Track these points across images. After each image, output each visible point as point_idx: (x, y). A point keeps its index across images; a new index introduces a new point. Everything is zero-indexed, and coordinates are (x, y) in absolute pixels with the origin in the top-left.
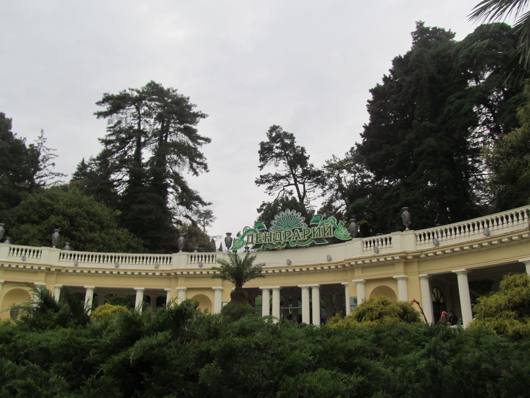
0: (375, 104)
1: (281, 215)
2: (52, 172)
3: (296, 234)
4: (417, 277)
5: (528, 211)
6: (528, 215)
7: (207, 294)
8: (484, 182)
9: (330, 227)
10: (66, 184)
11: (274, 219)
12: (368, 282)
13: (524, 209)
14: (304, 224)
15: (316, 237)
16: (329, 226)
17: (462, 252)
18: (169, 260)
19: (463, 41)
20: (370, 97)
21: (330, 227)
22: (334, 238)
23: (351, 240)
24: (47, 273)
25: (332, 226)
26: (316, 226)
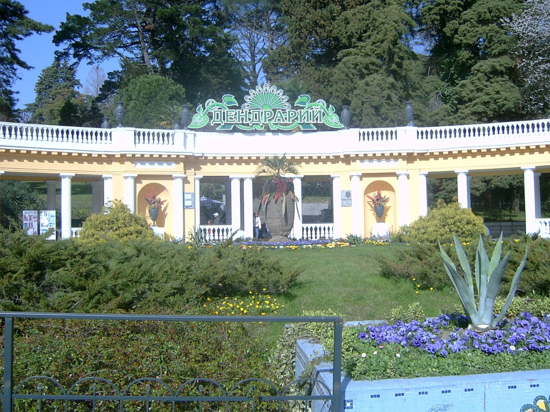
0: (513, 288)
1: (278, 92)
2: (377, 398)
3: (279, 115)
5: (548, 125)
6: (548, 128)
8: (325, 246)
9: (320, 112)
10: (415, 125)
11: (284, 95)
13: (545, 121)
14: (287, 104)
15: (315, 122)
16: (318, 110)
19: (494, 121)
20: (54, 44)
21: (320, 112)
22: (324, 124)
25: (322, 111)
26: (303, 108)
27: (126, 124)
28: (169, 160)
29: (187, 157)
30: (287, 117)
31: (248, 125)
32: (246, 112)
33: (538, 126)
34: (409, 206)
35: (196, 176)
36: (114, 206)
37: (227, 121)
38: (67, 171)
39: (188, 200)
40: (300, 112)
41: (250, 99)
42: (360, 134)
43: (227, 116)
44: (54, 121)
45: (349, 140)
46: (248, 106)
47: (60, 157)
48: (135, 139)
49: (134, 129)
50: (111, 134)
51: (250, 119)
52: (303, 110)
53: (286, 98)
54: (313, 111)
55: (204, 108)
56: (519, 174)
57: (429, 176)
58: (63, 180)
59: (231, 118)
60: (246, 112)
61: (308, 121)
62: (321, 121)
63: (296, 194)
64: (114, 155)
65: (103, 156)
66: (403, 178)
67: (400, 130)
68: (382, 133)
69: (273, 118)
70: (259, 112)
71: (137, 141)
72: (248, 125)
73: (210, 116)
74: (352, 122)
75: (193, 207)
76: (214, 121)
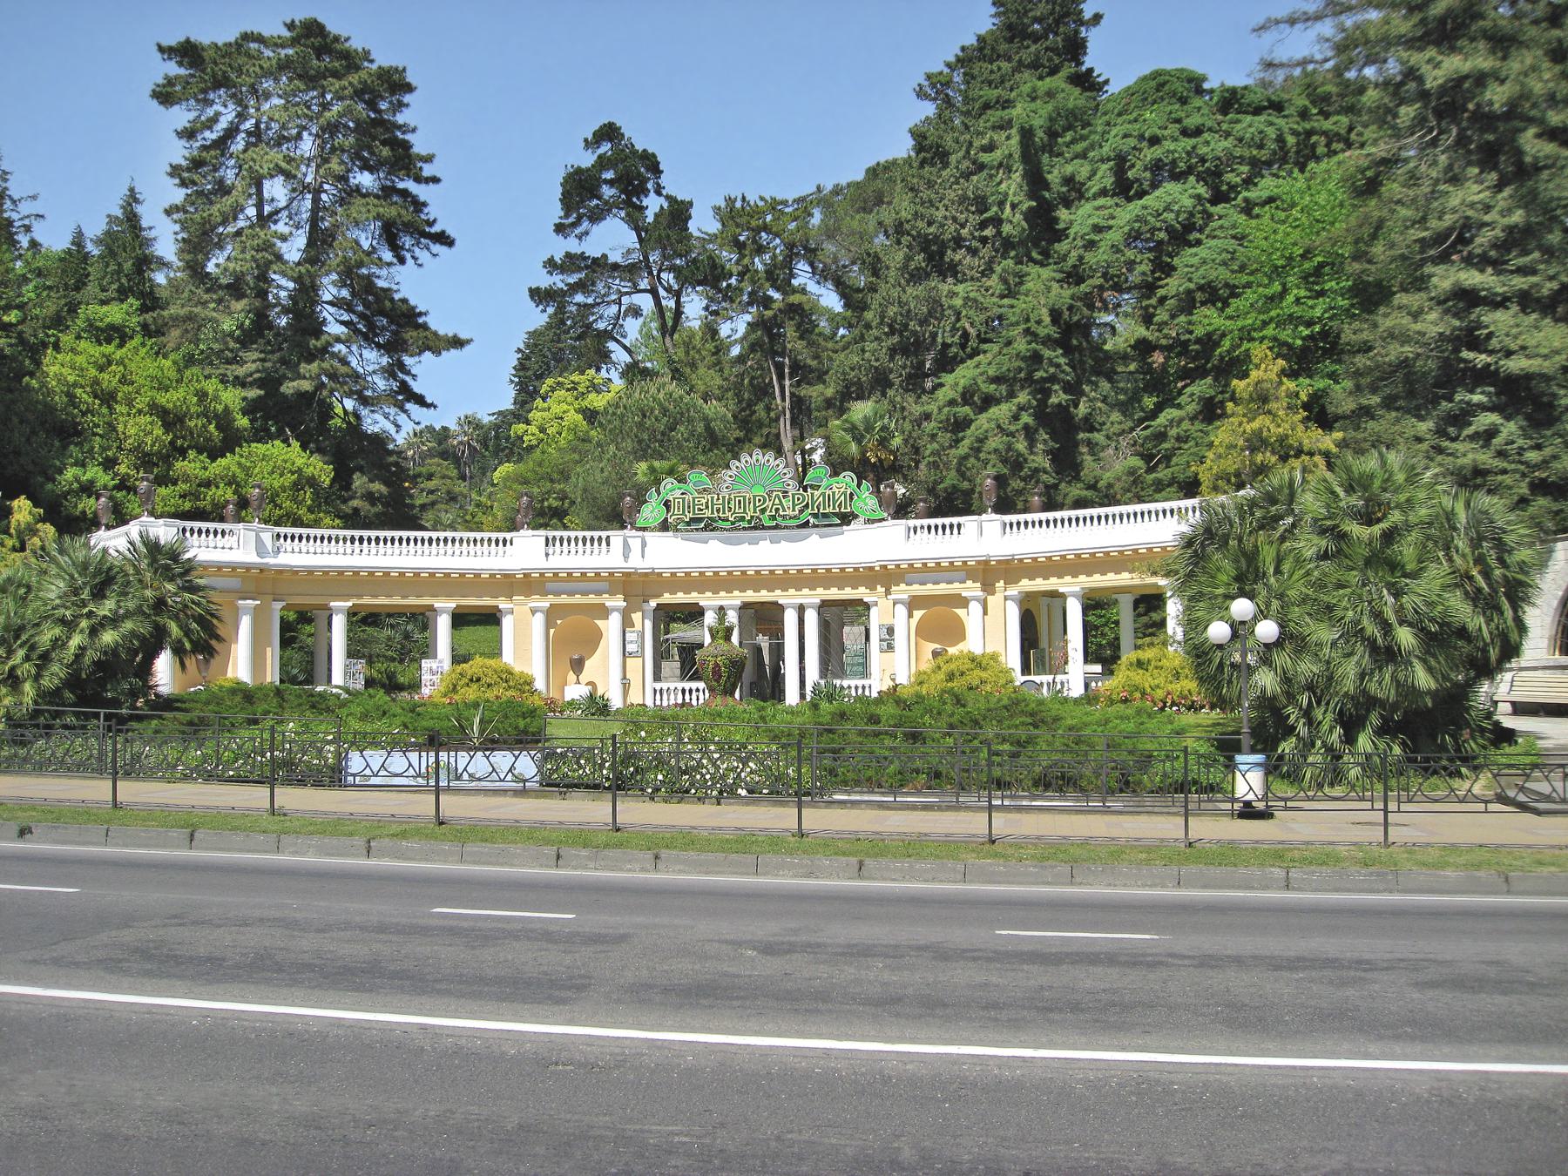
12: (913, 604)
66: (975, 607)
73: (667, 504)
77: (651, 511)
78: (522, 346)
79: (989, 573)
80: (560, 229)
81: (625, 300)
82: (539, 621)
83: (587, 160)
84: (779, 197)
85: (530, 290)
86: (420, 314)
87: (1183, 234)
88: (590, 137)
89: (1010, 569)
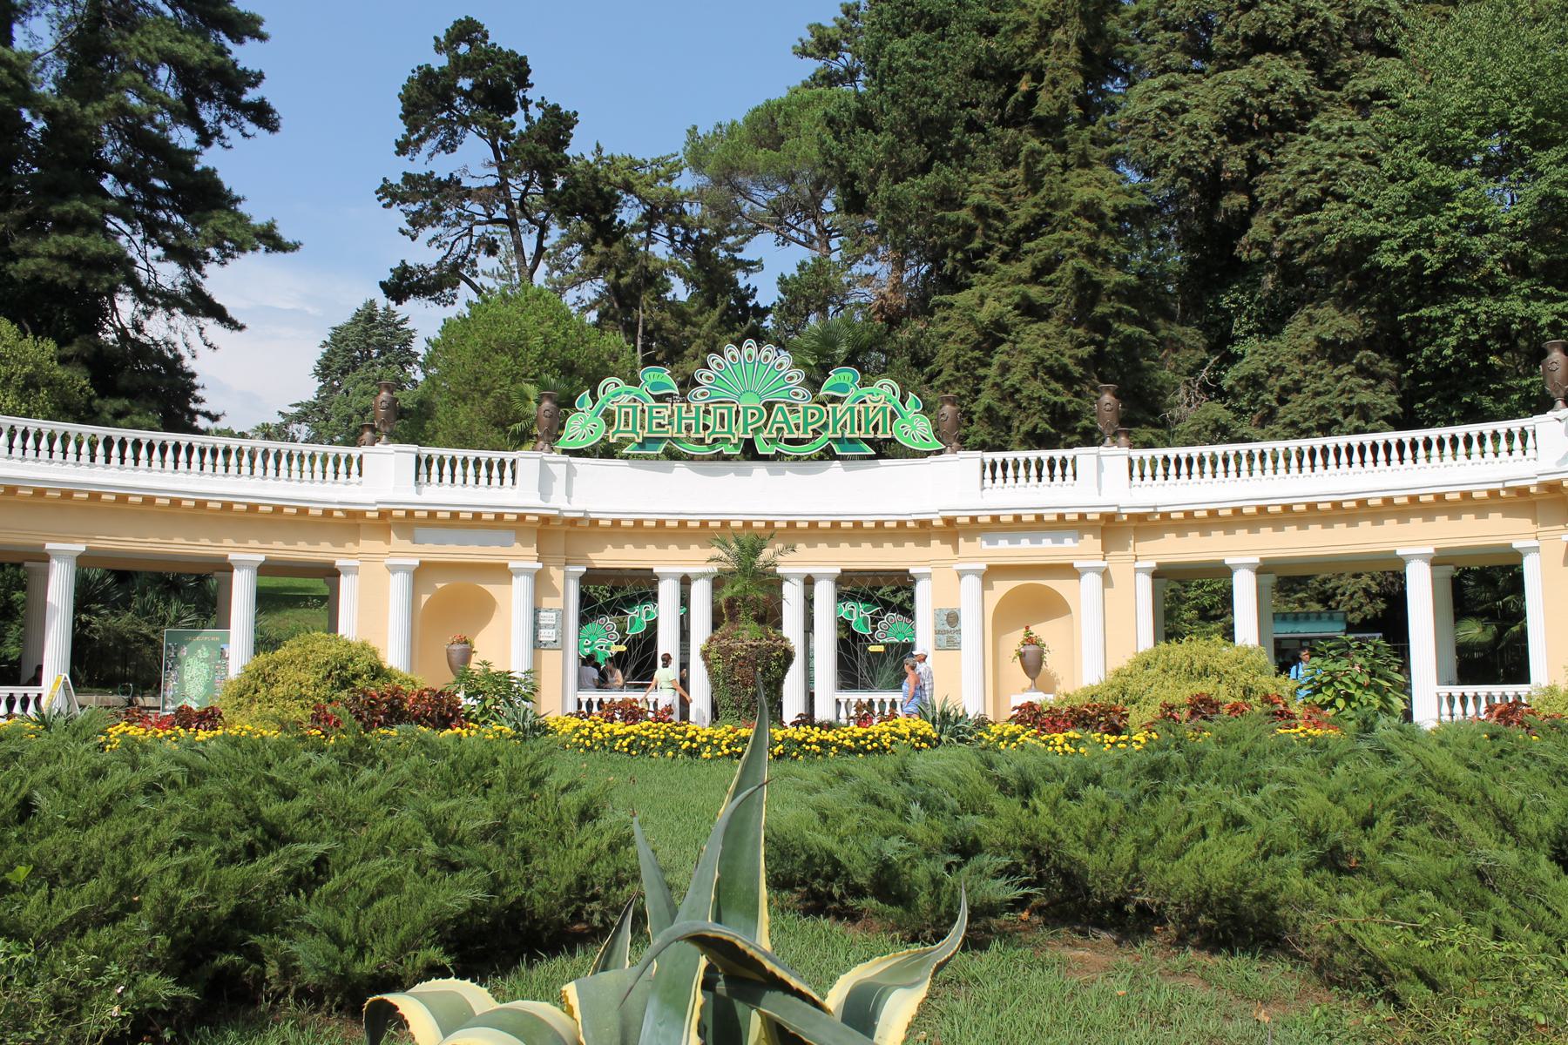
3: (780, 418)
4: (1131, 568)
7: (1059, 585)
9: (884, 410)
11: (722, 354)
12: (993, 573)
15: (871, 436)
16: (880, 405)
17: (1261, 518)
18: (508, 472)
21: (884, 410)
23: (939, 452)
24: (1104, 530)
25: (890, 407)
27: (395, 438)
28: (1061, 525)
29: (545, 520)
30: (801, 421)
31: (701, 441)
32: (698, 408)
33: (1226, 461)
34: (1103, 635)
35: (1138, 565)
36: (181, 963)
37: (650, 431)
38: (1417, 546)
39: (546, 626)
40: (834, 409)
41: (708, 378)
42: (984, 467)
43: (651, 418)
44: (122, 422)
45: (952, 482)
46: (703, 394)
47: (1388, 509)
48: (417, 474)
49: (414, 448)
50: (513, 462)
51: (706, 427)
52: (838, 405)
53: (799, 375)
54: (867, 409)
55: (595, 400)
56: (1223, 572)
57: (1160, 574)
58: (786, 587)
59: (660, 425)
60: (698, 408)
61: (852, 432)
62: (884, 432)
63: (786, 633)
64: (364, 512)
65: (336, 514)
66: (1091, 582)
67: (1084, 456)
68: (1027, 463)
69: (765, 425)
70: (730, 410)
71: (423, 478)
72: (701, 441)
73: (609, 417)
74: (958, 436)
75: (559, 645)
76: (618, 431)
77: (583, 425)
78: (328, 339)
79: (1113, 528)
80: (402, 148)
81: (478, 230)
82: (398, 587)
83: (440, 62)
84: (639, 158)
85: (398, 154)
86: (238, 200)
87: (1294, 119)
88: (442, 36)
89: (1146, 524)
